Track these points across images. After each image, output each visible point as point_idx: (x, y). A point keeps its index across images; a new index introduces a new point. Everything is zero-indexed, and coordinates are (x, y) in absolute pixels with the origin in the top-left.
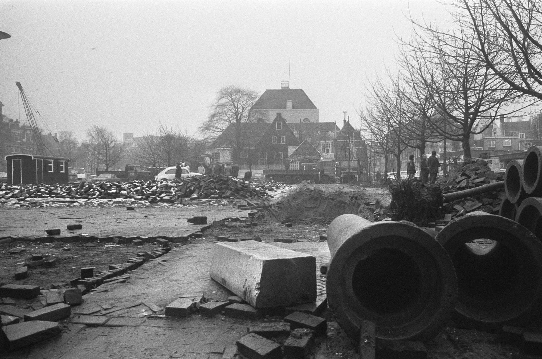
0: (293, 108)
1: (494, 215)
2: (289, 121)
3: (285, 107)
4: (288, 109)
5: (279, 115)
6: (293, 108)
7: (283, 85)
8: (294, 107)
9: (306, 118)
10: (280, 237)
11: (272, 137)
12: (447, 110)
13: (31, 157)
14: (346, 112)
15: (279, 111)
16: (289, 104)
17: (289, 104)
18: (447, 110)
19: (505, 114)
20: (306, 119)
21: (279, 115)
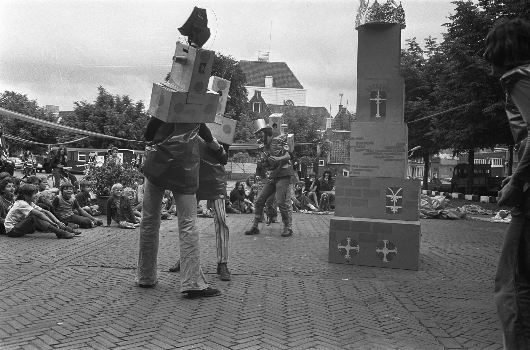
0: (273, 87)
1: (403, 222)
2: (267, 102)
3: (263, 85)
4: (267, 87)
5: (258, 93)
6: (273, 87)
7: (261, 57)
8: (275, 85)
9: (290, 100)
10: (370, 330)
11: (120, 182)
12: (28, 152)
13: (132, 152)
14: (343, 95)
15: (258, 89)
16: (269, 80)
17: (269, 80)
18: (28, 152)
19: (14, 333)
20: (290, 101)
21: (258, 93)
